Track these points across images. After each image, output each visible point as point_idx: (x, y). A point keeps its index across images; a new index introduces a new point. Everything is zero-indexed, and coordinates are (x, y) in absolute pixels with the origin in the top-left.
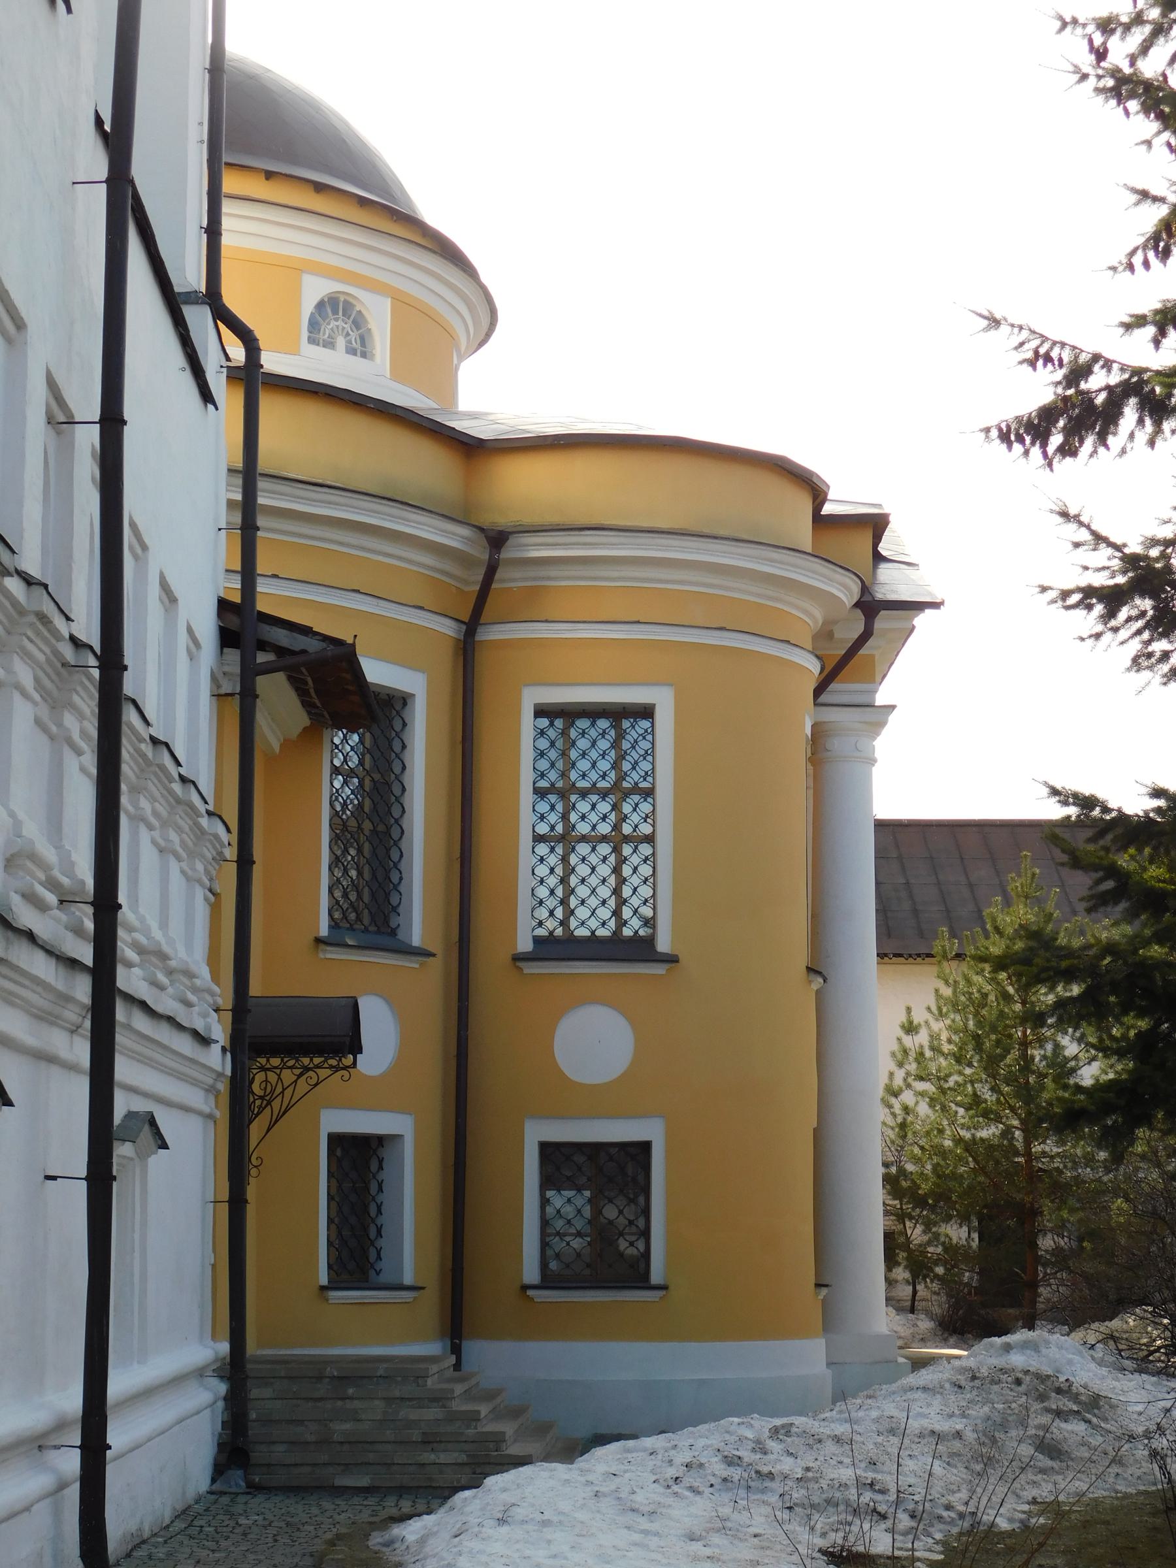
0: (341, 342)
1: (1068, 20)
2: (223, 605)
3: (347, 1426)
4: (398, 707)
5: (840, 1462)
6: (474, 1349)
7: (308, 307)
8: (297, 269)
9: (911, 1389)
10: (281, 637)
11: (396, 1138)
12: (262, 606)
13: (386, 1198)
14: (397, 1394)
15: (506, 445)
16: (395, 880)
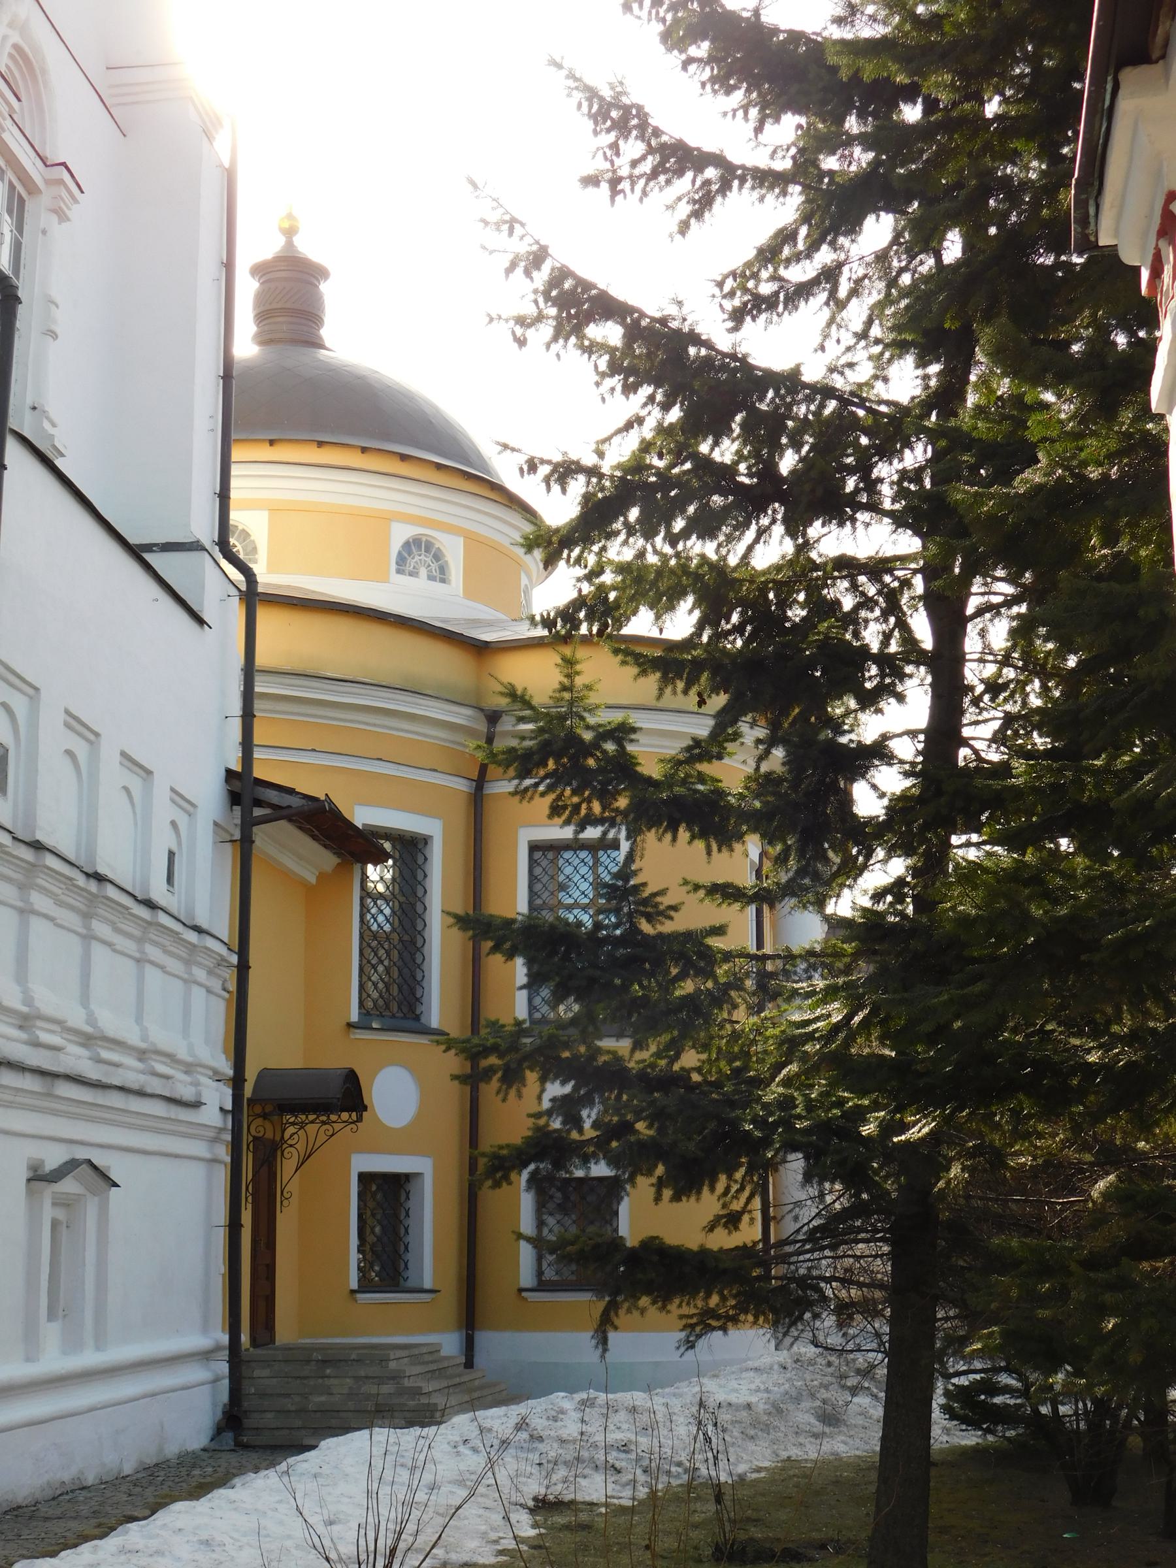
0: (423, 572)
1: (494, 316)
2: (230, 773)
3: (323, 1398)
4: (420, 846)
5: (619, 1428)
6: (491, 1343)
7: (396, 546)
8: (387, 518)
9: (747, 1370)
10: (273, 796)
11: (418, 1175)
12: (259, 773)
13: (411, 1222)
14: (363, 1373)
15: (504, 645)
16: (419, 978)
